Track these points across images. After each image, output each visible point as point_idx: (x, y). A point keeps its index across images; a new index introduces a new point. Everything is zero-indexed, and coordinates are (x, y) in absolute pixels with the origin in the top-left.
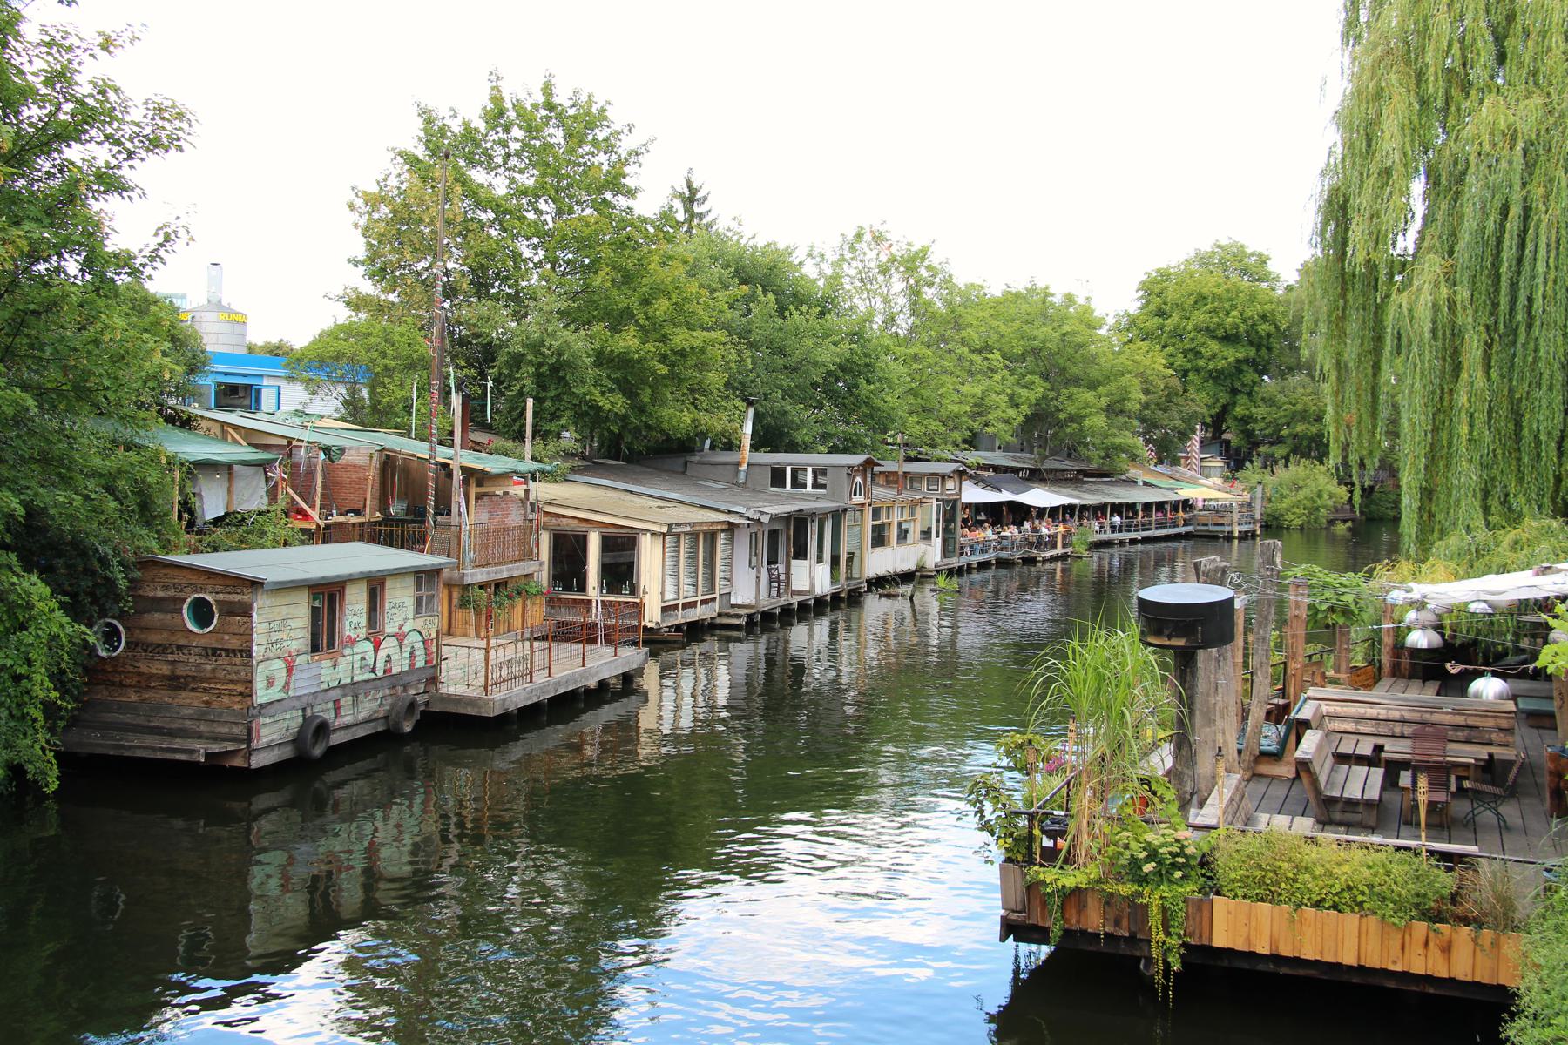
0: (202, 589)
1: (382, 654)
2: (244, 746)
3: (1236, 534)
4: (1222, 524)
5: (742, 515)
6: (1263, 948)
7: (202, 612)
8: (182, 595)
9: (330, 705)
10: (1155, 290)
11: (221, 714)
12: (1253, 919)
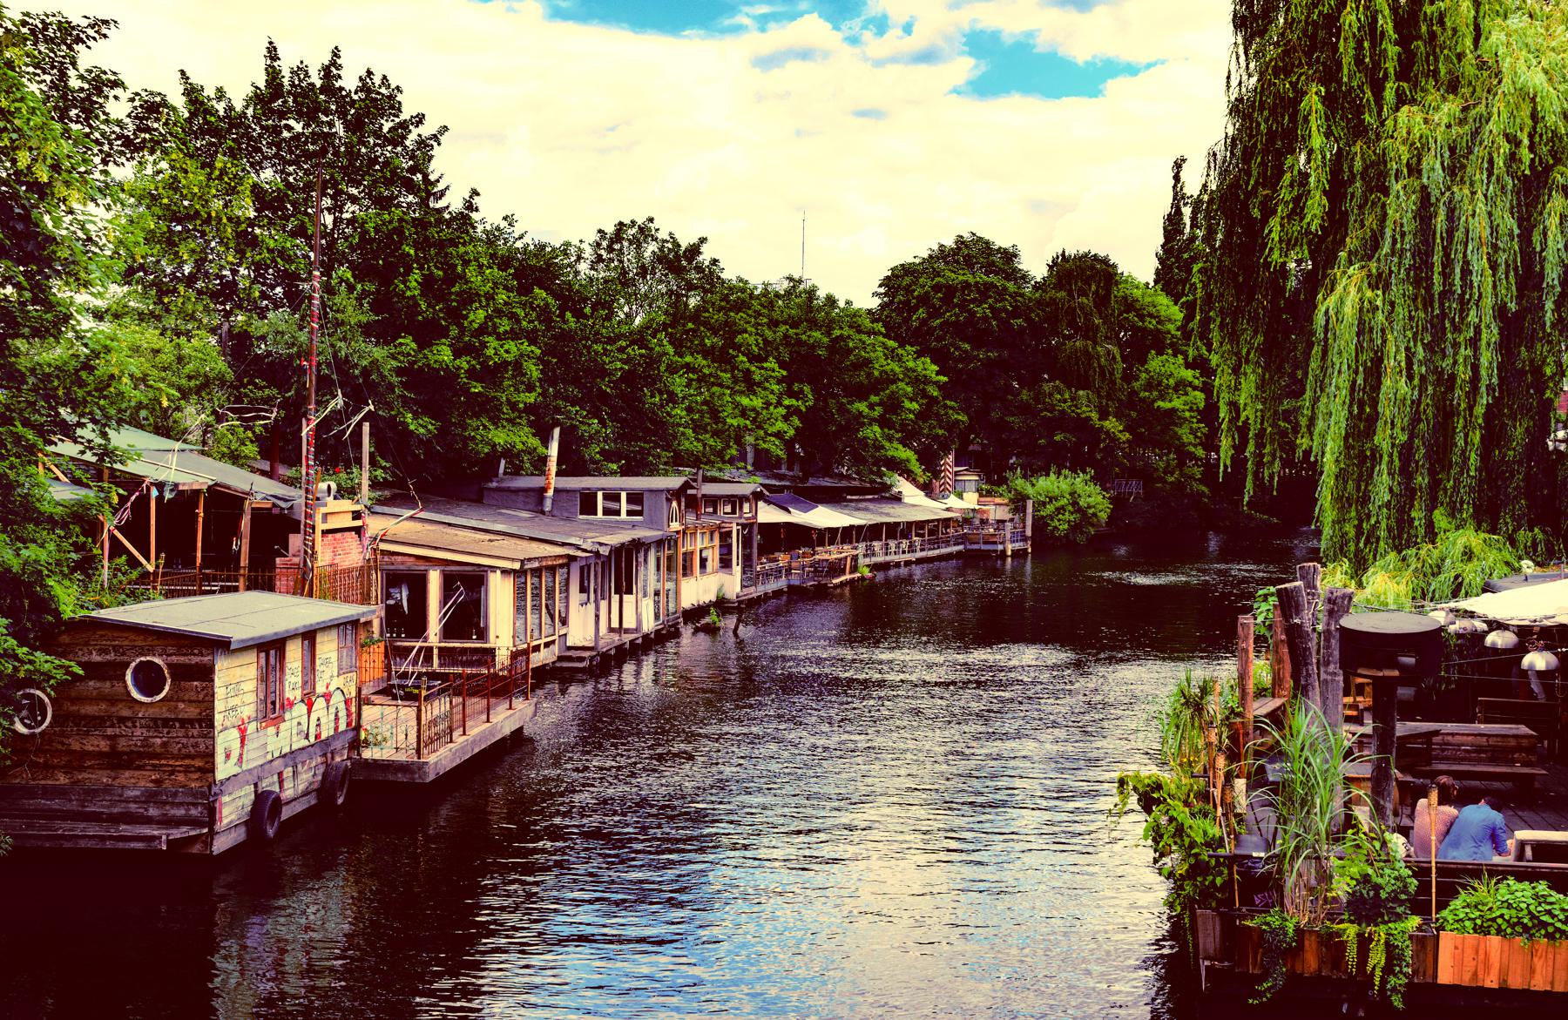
0: (151, 651)
1: (314, 717)
2: (206, 830)
3: (1009, 553)
4: (995, 543)
5: (578, 547)
6: (1491, 982)
7: (149, 679)
8: (125, 658)
9: (276, 778)
10: (899, 282)
11: (175, 794)
12: (1481, 952)
